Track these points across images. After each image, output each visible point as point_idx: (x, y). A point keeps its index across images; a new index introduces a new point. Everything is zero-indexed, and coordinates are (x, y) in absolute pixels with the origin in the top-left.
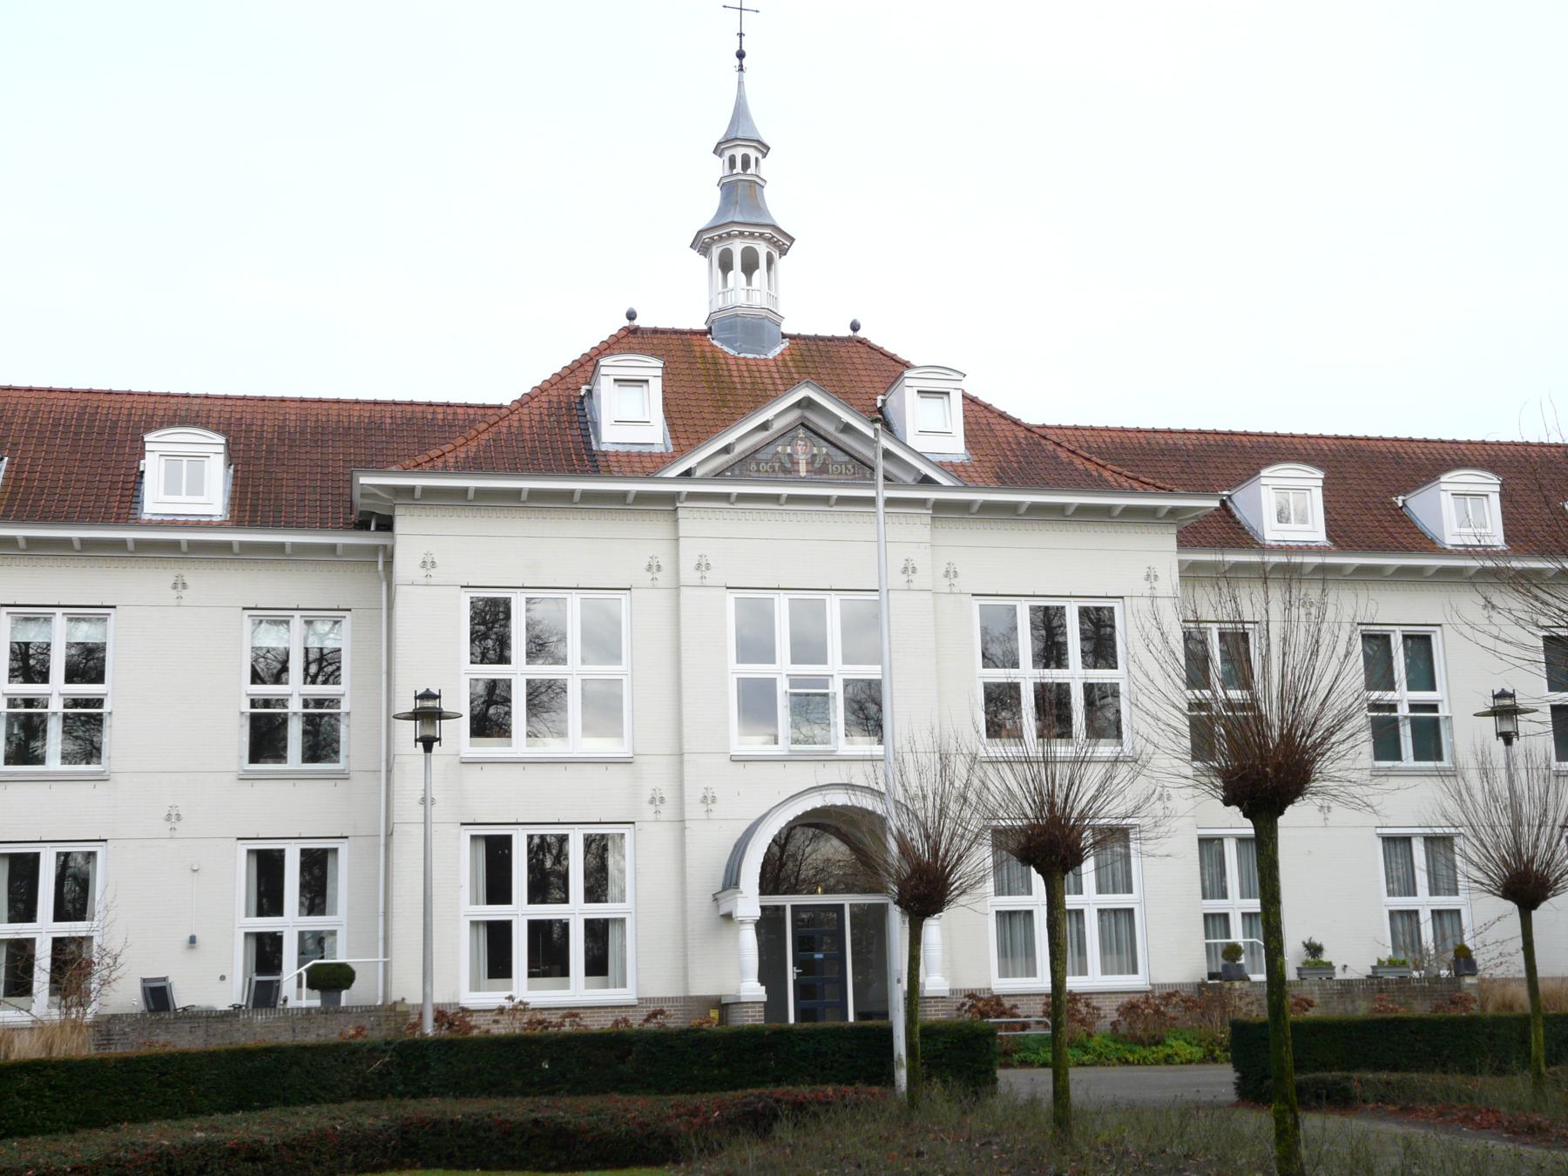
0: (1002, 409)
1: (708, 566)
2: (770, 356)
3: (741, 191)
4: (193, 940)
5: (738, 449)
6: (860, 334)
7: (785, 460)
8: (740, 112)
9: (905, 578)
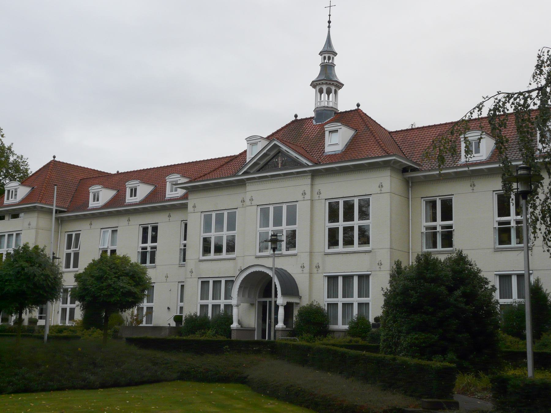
3: (327, 68)
4: (169, 308)
8: (329, 41)
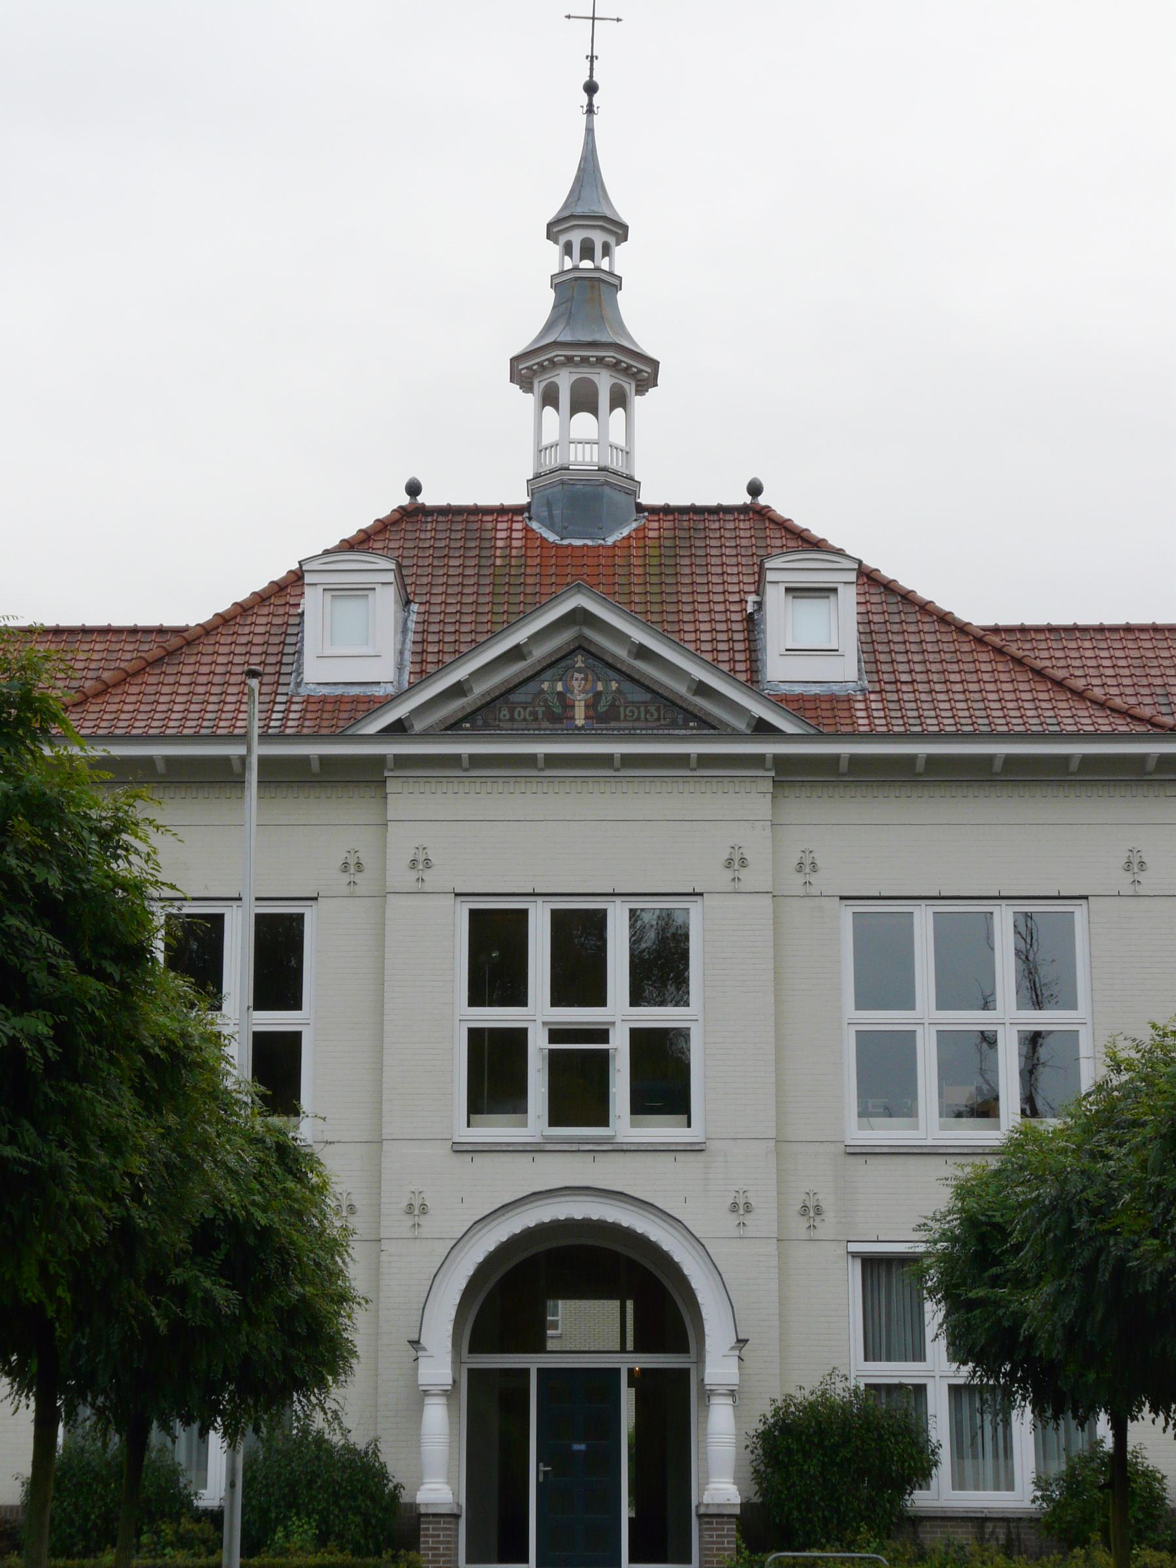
0: (946, 608)
1: (743, 862)
2: (610, 541)
3: (585, 295)
5: (480, 689)
6: (762, 500)
7: (554, 701)
8: (588, 171)
9: (729, 874)
